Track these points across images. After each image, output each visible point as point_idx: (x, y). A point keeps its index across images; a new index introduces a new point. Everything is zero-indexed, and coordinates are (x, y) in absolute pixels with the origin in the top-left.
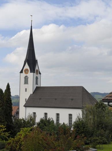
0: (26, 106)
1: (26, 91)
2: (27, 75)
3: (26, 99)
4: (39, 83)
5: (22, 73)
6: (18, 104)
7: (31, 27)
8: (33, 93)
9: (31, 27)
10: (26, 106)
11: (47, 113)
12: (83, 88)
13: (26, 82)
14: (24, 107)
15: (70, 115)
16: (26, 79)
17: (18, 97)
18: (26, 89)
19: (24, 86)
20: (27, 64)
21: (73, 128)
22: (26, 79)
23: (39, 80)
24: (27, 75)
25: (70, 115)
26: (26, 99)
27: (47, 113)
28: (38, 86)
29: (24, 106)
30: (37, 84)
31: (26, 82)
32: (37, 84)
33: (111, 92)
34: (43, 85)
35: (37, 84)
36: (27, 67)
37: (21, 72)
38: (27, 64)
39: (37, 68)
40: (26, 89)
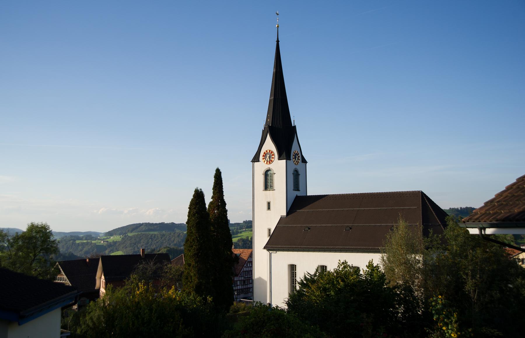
0: (271, 246)
1: (269, 208)
2: (271, 166)
3: (270, 230)
4: (301, 187)
5: (259, 161)
6: (248, 244)
7: (278, 41)
8: (288, 213)
9: (278, 41)
10: (271, 246)
11: (295, 266)
12: (423, 196)
13: (268, 185)
14: (265, 250)
15: (293, 268)
16: (267, 175)
17: (249, 225)
18: (269, 204)
19: (262, 196)
20: (268, 138)
21: (415, 282)
22: (267, 175)
23: (301, 178)
24: (271, 166)
25: (293, 268)
26: (270, 230)
27: (295, 266)
28: (299, 194)
29: (265, 248)
30: (298, 190)
31: (268, 185)
32: (296, 187)
33: (524, 174)
34: (312, 190)
35: (296, 187)
36: (269, 145)
37: (256, 159)
38: (269, 138)
39: (294, 149)
40: (269, 204)
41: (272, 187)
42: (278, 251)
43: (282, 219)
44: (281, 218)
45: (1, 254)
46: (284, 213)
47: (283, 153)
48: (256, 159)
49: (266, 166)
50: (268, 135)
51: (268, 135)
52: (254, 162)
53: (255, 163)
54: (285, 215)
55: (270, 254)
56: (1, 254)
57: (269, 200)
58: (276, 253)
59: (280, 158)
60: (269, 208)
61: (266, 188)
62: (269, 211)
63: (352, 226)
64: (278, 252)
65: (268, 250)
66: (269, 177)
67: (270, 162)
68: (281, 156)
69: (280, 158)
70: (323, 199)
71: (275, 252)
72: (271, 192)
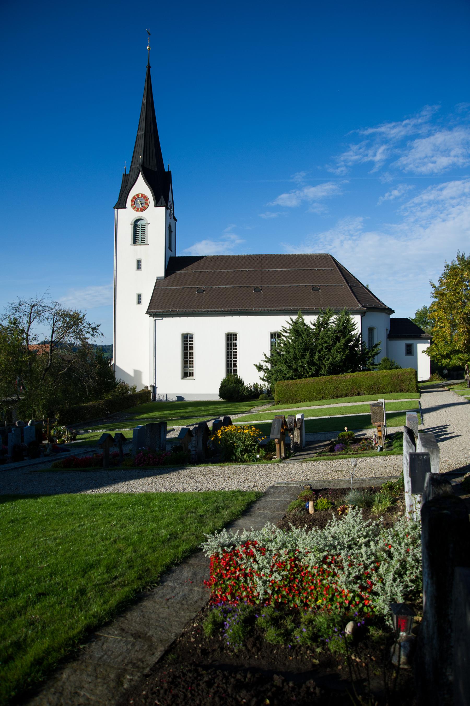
5: (125, 207)
23: (173, 234)
41: (143, 241)
42: (165, 317)
43: (159, 281)
44: (157, 279)
45: (387, 705)
46: (162, 274)
47: (161, 197)
48: (121, 204)
49: (137, 215)
50: (140, 174)
51: (140, 174)
52: (118, 208)
53: (119, 210)
54: (163, 275)
55: (155, 321)
56: (387, 705)
57: (139, 258)
58: (162, 319)
59: (157, 205)
60: (139, 267)
61: (135, 242)
62: (139, 272)
63: (261, 287)
64: (164, 318)
65: (151, 316)
66: (139, 229)
67: (143, 209)
68: (159, 201)
69: (157, 205)
70: (202, 260)
71: (161, 318)
72: (143, 247)
